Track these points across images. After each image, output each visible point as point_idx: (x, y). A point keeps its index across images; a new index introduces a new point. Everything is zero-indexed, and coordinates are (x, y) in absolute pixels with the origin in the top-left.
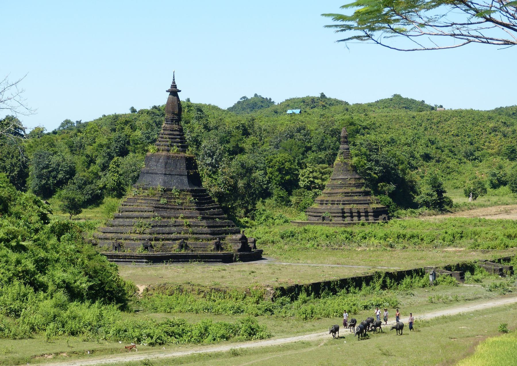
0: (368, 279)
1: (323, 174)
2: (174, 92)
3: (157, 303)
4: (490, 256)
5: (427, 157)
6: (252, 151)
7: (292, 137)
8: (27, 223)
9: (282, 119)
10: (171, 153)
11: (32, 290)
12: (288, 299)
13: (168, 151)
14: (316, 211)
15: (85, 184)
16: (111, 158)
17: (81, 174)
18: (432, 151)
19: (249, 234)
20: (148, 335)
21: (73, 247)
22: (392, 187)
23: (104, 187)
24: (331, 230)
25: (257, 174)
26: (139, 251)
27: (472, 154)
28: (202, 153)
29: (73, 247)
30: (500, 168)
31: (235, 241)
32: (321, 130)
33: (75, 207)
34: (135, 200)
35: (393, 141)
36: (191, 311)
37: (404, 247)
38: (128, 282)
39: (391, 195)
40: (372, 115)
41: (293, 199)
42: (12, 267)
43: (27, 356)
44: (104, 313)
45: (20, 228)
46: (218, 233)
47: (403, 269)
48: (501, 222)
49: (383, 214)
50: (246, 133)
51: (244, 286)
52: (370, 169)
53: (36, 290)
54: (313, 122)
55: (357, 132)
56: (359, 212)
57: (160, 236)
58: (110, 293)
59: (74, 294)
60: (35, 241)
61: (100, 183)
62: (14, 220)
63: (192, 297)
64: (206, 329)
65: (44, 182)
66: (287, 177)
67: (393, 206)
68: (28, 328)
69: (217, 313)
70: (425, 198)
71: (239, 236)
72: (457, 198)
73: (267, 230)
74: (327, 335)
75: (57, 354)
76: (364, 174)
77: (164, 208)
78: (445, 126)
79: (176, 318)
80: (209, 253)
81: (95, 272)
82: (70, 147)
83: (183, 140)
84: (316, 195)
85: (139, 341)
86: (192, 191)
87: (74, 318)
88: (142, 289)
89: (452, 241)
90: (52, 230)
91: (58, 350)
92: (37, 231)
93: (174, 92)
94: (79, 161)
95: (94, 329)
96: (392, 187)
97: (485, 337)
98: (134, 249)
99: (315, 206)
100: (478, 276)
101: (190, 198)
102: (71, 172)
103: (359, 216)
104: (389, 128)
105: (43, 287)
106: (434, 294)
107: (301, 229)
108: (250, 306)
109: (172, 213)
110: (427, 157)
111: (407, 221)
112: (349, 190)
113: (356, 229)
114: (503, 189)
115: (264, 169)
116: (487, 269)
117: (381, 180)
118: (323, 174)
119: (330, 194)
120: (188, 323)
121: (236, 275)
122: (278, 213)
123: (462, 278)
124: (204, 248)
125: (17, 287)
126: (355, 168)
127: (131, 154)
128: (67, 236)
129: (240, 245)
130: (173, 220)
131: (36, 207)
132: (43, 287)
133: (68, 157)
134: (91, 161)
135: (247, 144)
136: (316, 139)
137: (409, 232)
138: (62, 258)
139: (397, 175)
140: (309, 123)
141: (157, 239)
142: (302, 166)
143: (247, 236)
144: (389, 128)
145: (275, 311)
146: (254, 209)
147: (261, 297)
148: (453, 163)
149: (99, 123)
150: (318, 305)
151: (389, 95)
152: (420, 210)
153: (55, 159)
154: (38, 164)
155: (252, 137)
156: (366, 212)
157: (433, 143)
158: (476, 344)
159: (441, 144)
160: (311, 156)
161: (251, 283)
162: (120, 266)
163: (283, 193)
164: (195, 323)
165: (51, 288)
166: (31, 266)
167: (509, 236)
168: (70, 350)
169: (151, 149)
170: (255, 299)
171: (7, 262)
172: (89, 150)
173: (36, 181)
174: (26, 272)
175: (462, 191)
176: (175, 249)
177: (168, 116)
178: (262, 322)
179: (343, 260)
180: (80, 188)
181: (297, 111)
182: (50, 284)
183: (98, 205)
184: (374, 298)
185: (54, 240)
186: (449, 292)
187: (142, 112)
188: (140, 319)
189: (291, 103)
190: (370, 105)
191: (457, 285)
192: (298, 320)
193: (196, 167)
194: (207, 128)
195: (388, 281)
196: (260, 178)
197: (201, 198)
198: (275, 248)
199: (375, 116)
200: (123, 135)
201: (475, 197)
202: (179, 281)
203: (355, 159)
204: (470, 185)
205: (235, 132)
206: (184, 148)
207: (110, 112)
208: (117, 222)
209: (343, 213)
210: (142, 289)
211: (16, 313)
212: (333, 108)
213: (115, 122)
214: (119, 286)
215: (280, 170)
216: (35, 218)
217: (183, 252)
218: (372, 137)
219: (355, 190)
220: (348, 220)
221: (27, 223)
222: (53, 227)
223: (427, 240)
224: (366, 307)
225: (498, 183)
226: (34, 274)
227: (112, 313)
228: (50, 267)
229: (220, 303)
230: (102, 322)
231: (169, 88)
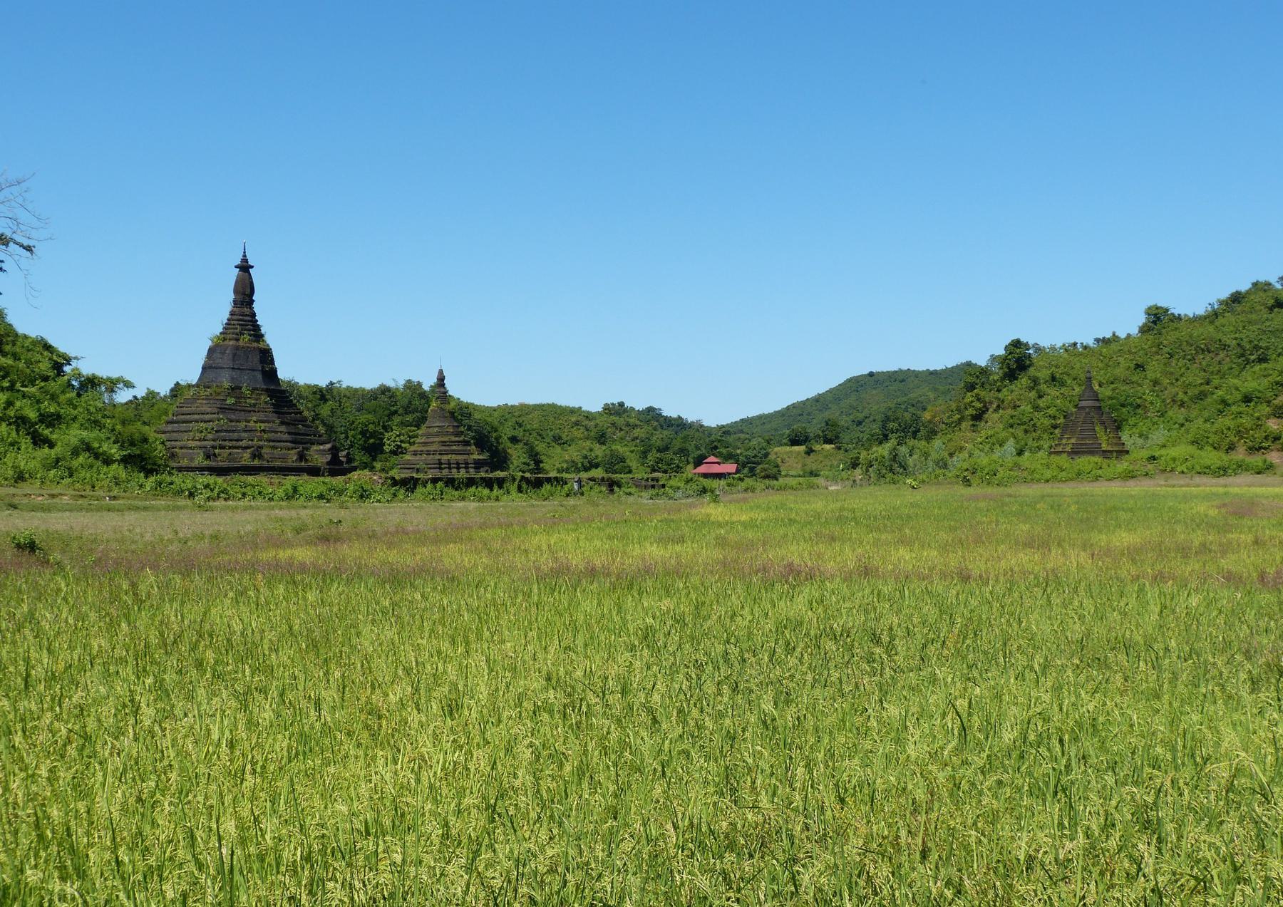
7: (375, 399)
10: (241, 343)
13: (237, 340)
18: (519, 433)
26: (199, 460)
30: (591, 450)
31: (322, 452)
41: (378, 465)
56: (458, 464)
66: (372, 441)
77: (231, 409)
80: (290, 464)
85: (191, 495)
86: (267, 390)
98: (192, 459)
101: (265, 398)
109: (242, 415)
112: (446, 439)
115: (346, 432)
119: (425, 444)
124: (284, 458)
129: (329, 457)
130: (243, 424)
131: (46, 353)
141: (222, 447)
142: (386, 428)
156: (467, 463)
157: (520, 426)
160: (397, 419)
163: (366, 458)
176: (246, 458)
208: (170, 427)
209: (440, 463)
215: (363, 433)
217: (256, 462)
219: (454, 439)
231: (238, 262)
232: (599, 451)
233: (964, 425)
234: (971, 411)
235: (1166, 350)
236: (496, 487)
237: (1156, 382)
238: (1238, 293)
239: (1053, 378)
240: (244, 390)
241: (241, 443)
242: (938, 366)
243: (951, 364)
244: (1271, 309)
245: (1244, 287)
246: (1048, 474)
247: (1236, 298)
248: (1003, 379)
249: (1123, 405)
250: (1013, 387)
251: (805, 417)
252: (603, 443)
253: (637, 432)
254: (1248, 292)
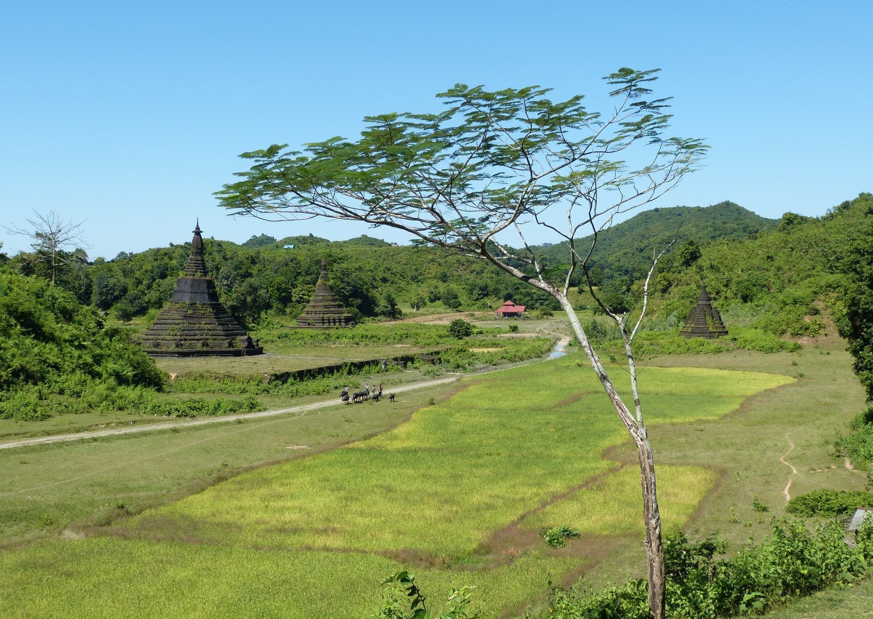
0: (338, 368)
1: (309, 292)
2: (198, 232)
3: (185, 386)
4: (425, 351)
5: (384, 280)
6: (258, 275)
7: (287, 265)
8: (87, 329)
9: (280, 252)
10: (196, 277)
11: (90, 377)
12: (280, 383)
14: (303, 319)
15: (135, 299)
16: (154, 280)
17: (132, 292)
18: (388, 275)
19: (253, 335)
20: (176, 410)
21: (121, 346)
22: (359, 301)
23: (149, 301)
24: (313, 332)
25: (262, 292)
27: (416, 278)
28: (220, 276)
29: (121, 346)
30: (436, 287)
31: (243, 341)
32: (308, 260)
33: (126, 316)
34: (169, 311)
35: (360, 268)
36: (209, 391)
37: (366, 345)
38: (163, 371)
39: (358, 307)
40: (345, 249)
41: (288, 310)
42: (75, 361)
43: (85, 425)
44: (144, 394)
45: (82, 331)
46: (230, 335)
47: (363, 360)
48: (435, 326)
49: (351, 321)
50: (253, 262)
51: (248, 373)
52: (343, 288)
53: (93, 377)
54: (303, 255)
55: (335, 261)
56: (334, 319)
57: (188, 337)
58: (150, 380)
59: (121, 380)
60: (93, 341)
61: (146, 299)
62: (77, 326)
63: (210, 382)
64: (219, 405)
65: (104, 297)
67: (360, 315)
68: (86, 405)
69: (228, 393)
70: (383, 309)
71: (246, 337)
72: (406, 309)
73: (268, 332)
74: (339, 401)
75: (108, 424)
76: (339, 292)
78: (398, 257)
79: (197, 397)
80: (224, 349)
81: (138, 364)
82: (124, 272)
83: (204, 267)
84: (304, 307)
85: (169, 414)
86: (211, 305)
87: (121, 398)
88: (173, 376)
89: (400, 340)
90: (106, 333)
91: (109, 421)
92: (94, 334)
93: (198, 232)
94: (130, 282)
95: (136, 406)
96: (359, 301)
97: (419, 407)
98: (168, 347)
99: (303, 315)
100: (417, 365)
101: (210, 310)
102: (125, 290)
103: (335, 322)
104: (357, 259)
105: (99, 375)
106: (385, 377)
107: (293, 331)
108: (252, 387)
109: (197, 321)
110: (384, 280)
111: (370, 326)
112: (327, 303)
113: (332, 332)
114: (438, 303)
116: (423, 360)
117: (351, 296)
118: (309, 292)
119: (314, 307)
120: (206, 400)
121: (243, 365)
122: (277, 320)
123: (405, 366)
124: (220, 346)
125: (79, 375)
126: (331, 288)
127: (169, 277)
128: (117, 337)
131: (93, 316)
132: (99, 375)
133: (122, 279)
134: (139, 282)
135: (254, 270)
136: (304, 266)
137: (370, 334)
138: (114, 354)
139: (362, 292)
140: (299, 255)
143: (252, 337)
144: (357, 259)
145: (271, 391)
146: (259, 317)
147: (260, 381)
148: (403, 284)
149: (145, 255)
150: (302, 386)
151: (359, 236)
152: (379, 318)
153: (112, 281)
154: (100, 284)
155: (258, 265)
156: (340, 319)
157: (389, 270)
158: (412, 413)
159: (394, 271)
160: (300, 279)
161: (253, 371)
162: (157, 359)
163: (280, 306)
164: (211, 400)
165: (105, 376)
166: (89, 360)
167: (440, 336)
168: (117, 421)
169: (181, 274)
170: (256, 383)
171: (71, 357)
172: (138, 274)
173: (98, 297)
174: (86, 364)
175: (409, 304)
176: (199, 346)
177: (195, 250)
178: (261, 399)
179: (321, 354)
180: (131, 302)
181: (292, 247)
182: (104, 373)
183: (144, 315)
184: (342, 381)
185: (107, 341)
186: (396, 377)
187: (177, 246)
188: (171, 398)
189: (288, 241)
190: (345, 242)
191: (401, 371)
192: (286, 397)
193: (214, 287)
194: (225, 258)
195: (353, 369)
196: (264, 295)
197: (218, 310)
198: (273, 346)
199: (348, 250)
200: (163, 263)
202: (201, 370)
203: (331, 281)
204: (414, 299)
205: (245, 261)
206: (205, 273)
207: (155, 246)
208: (156, 327)
210: (173, 376)
211: (78, 394)
212: (318, 244)
213: (157, 254)
214: (156, 374)
215: (278, 289)
216: (93, 325)
218: (345, 265)
219: (332, 303)
220: (326, 325)
221: (87, 329)
222: (106, 331)
223: (382, 339)
224: (336, 388)
225: (434, 298)
226: (92, 365)
227: (150, 394)
228: (104, 361)
229: (230, 386)
230: (142, 401)
231: (194, 229)
232: (442, 288)
234: (659, 287)
235: (791, 245)
237: (779, 269)
238: (847, 202)
239: (712, 267)
242: (704, 205)
243: (714, 203)
244: (866, 214)
245: (852, 196)
246: (672, 348)
247: (846, 206)
248: (682, 265)
249: (754, 285)
250: (688, 271)
251: (608, 241)
252: (444, 282)
254: (855, 201)
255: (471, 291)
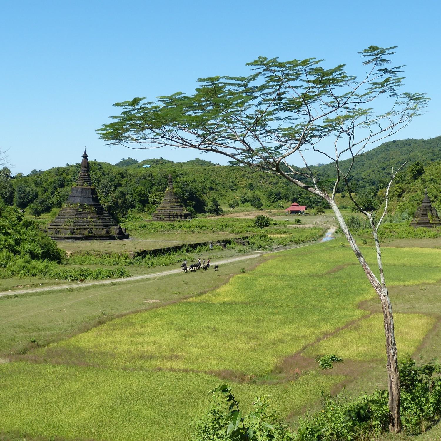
7: (145, 178)
10: (84, 187)
13: (83, 185)
18: (213, 185)
26: (68, 234)
30: (246, 193)
31: (116, 230)
41: (146, 209)
50: (123, 177)
66: (143, 198)
80: (103, 235)
85: (66, 279)
86: (94, 205)
98: (65, 234)
109: (84, 216)
110: (211, 189)
112: (172, 204)
114: (247, 204)
115: (132, 194)
117: (188, 199)
119: (163, 206)
124: (100, 233)
129: (118, 232)
131: (15, 213)
141: (77, 229)
142: (150, 193)
156: (181, 215)
157: (214, 182)
160: (154, 188)
176: (86, 233)
201: (234, 208)
208: (57, 220)
209: (170, 215)
215: (139, 195)
217: (90, 235)
219: (175, 204)
220: (172, 219)
233: (394, 198)
236: (178, 250)
239: (432, 180)
240: (85, 205)
241: (84, 227)
242: (426, 138)
248: (411, 179)
250: (415, 183)
252: (251, 190)
253: (271, 180)
255: (269, 196)
